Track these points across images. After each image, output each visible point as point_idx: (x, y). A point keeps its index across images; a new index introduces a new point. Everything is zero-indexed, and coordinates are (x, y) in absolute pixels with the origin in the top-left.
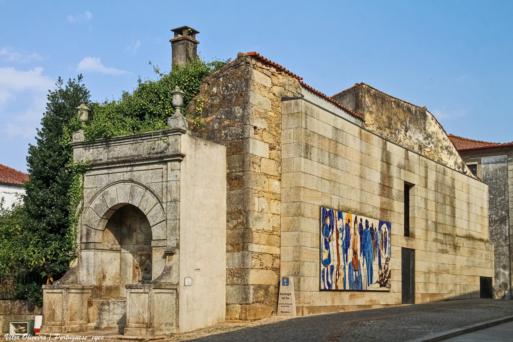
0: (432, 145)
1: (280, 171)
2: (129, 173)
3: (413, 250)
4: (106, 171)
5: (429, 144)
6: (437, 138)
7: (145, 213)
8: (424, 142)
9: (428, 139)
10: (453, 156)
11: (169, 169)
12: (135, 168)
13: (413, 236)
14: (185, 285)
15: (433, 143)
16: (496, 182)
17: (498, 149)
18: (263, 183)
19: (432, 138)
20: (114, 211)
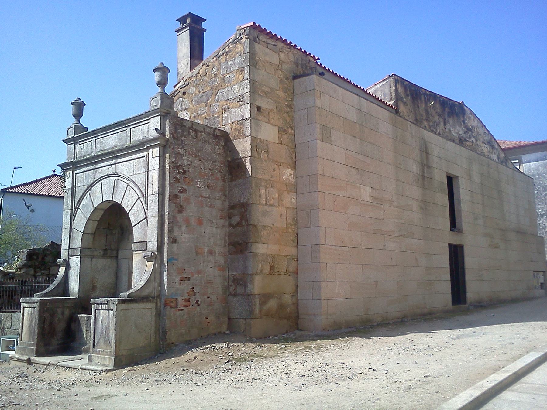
0: (473, 139)
1: (294, 158)
2: (113, 166)
3: (462, 247)
4: (154, 187)
5: (470, 138)
6: (478, 132)
7: (127, 210)
8: (464, 136)
9: (468, 133)
10: (495, 151)
11: (150, 157)
12: (119, 161)
13: (460, 231)
14: (544, 272)
15: (474, 137)
16: (539, 178)
17: (538, 146)
18: (272, 170)
19: (472, 132)
20: (102, 212)
